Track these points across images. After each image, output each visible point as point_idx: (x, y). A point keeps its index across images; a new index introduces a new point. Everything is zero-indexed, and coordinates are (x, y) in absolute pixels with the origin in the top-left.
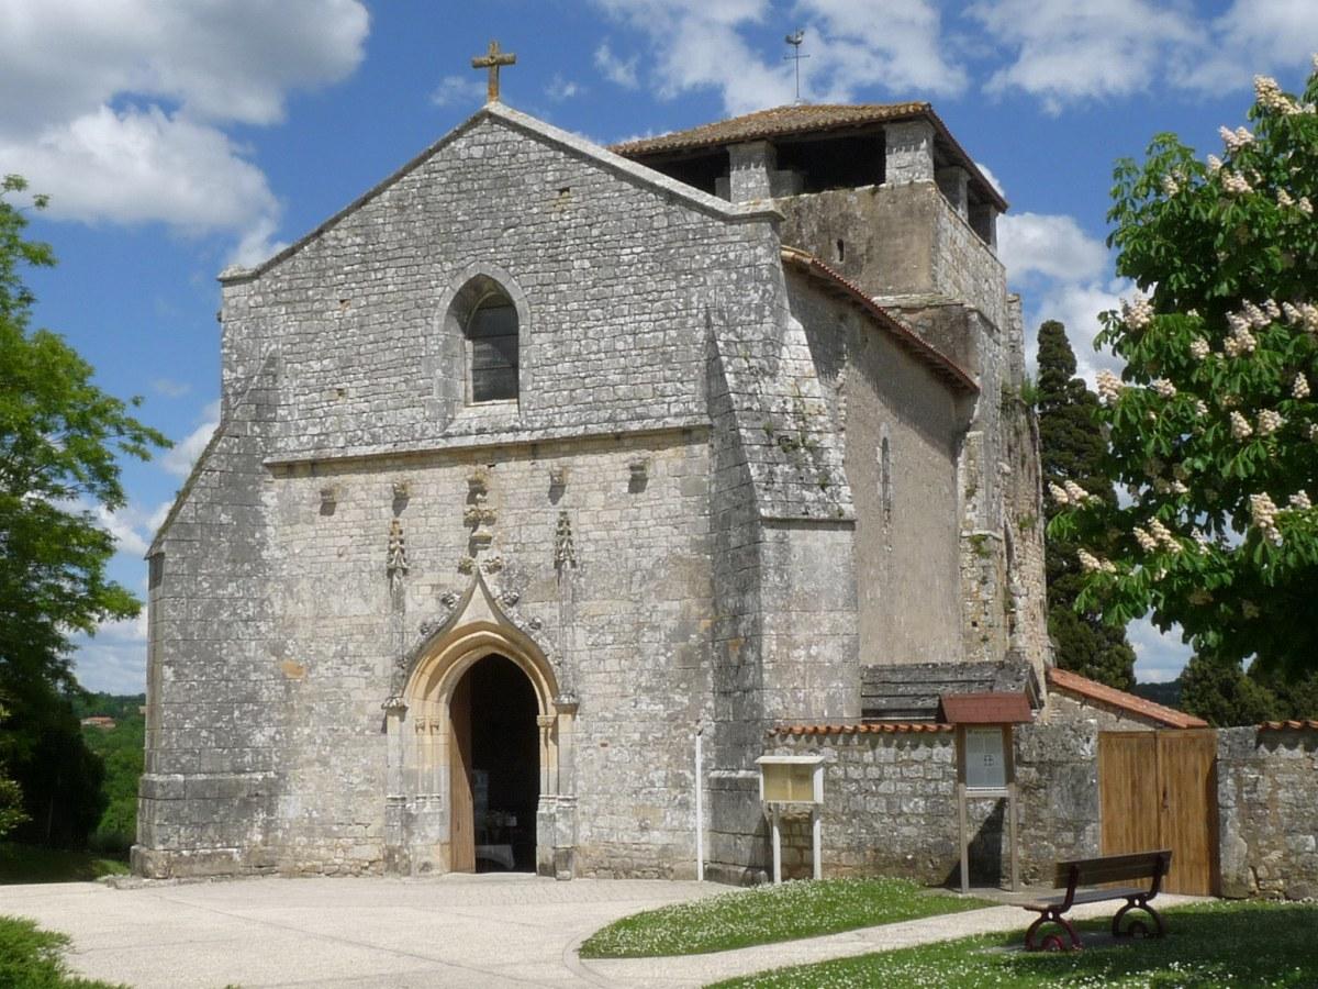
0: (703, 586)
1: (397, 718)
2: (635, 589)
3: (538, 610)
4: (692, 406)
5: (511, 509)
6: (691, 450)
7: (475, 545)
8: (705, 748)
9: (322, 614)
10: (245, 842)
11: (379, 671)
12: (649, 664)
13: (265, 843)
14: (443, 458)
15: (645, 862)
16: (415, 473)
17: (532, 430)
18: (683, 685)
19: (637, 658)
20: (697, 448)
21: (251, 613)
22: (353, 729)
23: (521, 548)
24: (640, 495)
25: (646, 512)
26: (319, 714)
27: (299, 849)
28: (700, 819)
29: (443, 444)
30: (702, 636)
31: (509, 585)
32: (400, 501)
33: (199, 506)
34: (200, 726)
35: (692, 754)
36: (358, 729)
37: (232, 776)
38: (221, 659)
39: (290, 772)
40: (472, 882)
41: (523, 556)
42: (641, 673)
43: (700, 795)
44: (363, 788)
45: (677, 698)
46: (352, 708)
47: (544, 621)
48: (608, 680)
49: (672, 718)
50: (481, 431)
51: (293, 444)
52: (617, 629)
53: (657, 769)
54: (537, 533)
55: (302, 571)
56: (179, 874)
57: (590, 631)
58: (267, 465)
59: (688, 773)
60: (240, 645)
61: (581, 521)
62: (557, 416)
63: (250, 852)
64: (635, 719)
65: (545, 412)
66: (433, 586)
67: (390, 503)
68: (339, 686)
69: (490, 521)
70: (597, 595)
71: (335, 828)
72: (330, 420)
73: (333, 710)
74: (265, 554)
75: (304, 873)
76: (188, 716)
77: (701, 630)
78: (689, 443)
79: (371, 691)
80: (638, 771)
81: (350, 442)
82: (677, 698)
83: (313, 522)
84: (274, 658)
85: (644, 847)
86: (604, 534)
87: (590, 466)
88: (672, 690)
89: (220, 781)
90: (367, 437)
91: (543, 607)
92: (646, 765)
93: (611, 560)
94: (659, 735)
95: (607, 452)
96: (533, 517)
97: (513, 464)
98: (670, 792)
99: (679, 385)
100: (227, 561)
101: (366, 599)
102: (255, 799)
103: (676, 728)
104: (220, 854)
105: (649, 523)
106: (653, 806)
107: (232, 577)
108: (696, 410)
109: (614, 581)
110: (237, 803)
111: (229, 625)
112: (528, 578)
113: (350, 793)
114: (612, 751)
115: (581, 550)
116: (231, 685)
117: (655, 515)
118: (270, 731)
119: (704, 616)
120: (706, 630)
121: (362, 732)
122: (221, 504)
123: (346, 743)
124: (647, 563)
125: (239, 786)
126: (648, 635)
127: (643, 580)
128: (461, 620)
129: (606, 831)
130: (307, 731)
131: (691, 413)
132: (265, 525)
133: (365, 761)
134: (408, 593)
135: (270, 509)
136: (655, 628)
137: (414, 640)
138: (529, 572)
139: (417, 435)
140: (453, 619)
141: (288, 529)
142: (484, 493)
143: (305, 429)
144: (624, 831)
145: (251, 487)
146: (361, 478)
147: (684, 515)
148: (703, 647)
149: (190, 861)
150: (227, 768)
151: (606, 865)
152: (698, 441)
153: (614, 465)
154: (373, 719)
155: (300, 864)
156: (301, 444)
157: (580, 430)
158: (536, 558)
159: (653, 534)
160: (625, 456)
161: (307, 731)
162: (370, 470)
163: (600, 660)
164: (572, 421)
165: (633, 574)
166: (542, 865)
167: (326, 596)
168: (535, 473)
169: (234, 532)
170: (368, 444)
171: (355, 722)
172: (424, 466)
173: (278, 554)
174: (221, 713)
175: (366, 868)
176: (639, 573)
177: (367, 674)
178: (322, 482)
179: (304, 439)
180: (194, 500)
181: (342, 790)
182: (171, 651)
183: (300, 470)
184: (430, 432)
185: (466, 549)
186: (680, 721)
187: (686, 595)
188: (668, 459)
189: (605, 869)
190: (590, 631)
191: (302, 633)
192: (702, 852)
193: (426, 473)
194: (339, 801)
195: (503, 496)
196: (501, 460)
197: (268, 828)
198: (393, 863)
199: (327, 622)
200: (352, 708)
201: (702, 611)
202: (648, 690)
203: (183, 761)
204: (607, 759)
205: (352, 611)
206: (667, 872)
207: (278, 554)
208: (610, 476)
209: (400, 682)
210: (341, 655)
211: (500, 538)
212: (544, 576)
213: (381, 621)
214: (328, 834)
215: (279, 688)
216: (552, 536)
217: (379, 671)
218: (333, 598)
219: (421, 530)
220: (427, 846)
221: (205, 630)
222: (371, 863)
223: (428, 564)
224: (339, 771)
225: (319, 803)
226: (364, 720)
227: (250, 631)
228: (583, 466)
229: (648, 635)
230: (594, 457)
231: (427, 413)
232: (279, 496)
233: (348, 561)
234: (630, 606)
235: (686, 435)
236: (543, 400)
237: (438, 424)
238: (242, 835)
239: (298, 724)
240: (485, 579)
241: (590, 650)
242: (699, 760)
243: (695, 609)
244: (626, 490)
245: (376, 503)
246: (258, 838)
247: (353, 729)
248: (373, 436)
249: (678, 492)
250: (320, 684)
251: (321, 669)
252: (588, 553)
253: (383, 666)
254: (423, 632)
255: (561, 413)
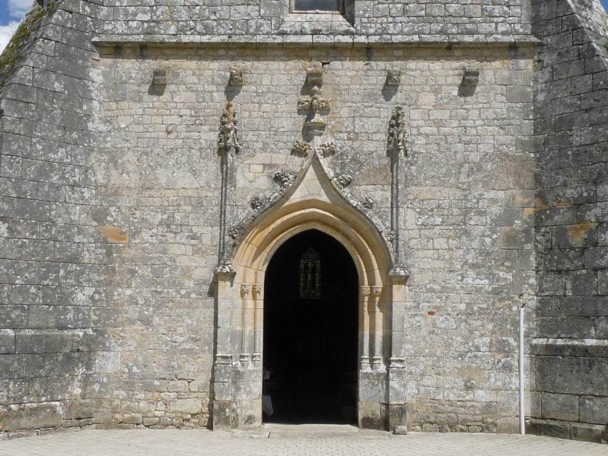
0: (529, 180)
1: (228, 283)
2: (463, 178)
3: (371, 192)
4: (518, 27)
5: (344, 102)
6: (517, 65)
7: (308, 132)
8: (528, 318)
9: (148, 184)
10: (67, 396)
11: (207, 240)
12: (476, 244)
13: (83, 396)
14: (278, 53)
15: (469, 417)
16: (248, 64)
17: (368, 35)
18: (507, 264)
19: (464, 238)
20: (522, 62)
21: (77, 179)
22: (178, 292)
23: (354, 136)
24: (469, 99)
25: (474, 114)
26: (142, 277)
27: (117, 402)
28: (523, 380)
29: (279, 39)
30: (524, 222)
31: (342, 168)
32: (233, 86)
33: (36, 71)
34: (30, 283)
35: (516, 324)
36: (183, 292)
37: (57, 333)
38: (50, 220)
39: (110, 330)
40: (334, 435)
41: (356, 144)
42: (467, 251)
43: (524, 360)
44: (188, 346)
45: (501, 274)
46: (178, 272)
47: (376, 202)
48: (436, 256)
49: (496, 292)
50: (315, 32)
51: (121, 27)
52: (446, 212)
53: (482, 335)
54: (370, 125)
55: (128, 145)
56: (7, 428)
57: (419, 213)
58: (95, 44)
59: (511, 340)
60: (66, 209)
61: (413, 117)
62: (391, 25)
63: (71, 406)
64: (461, 291)
65: (380, 20)
66: (265, 165)
67: (223, 88)
68: (164, 252)
69: (325, 111)
70: (427, 182)
71: (157, 383)
72: (161, 9)
73: (157, 273)
74: (90, 126)
75: (121, 425)
76: (19, 272)
77: (525, 217)
78: (515, 57)
79: (197, 258)
80: (463, 337)
81: (182, 31)
82: (501, 274)
83: (140, 100)
84: (94, 223)
85: (468, 404)
86: (435, 130)
87: (422, 71)
88: (497, 267)
89: (47, 336)
90: (199, 27)
91: (375, 190)
92: (471, 332)
93: (441, 152)
94: (484, 306)
95: (438, 60)
96: (367, 110)
97: (347, 63)
98: (493, 356)
99: (506, 8)
100: (59, 128)
101: (194, 173)
102: (76, 355)
103: (501, 300)
104: (44, 408)
105: (478, 122)
106: (478, 368)
107: (63, 143)
108: (521, 30)
109: (444, 171)
110: (60, 358)
111: (58, 188)
112: (361, 164)
113: (174, 349)
114: (439, 319)
115: (412, 143)
116: (58, 245)
117: (483, 116)
118: (89, 291)
119: (528, 205)
120: (530, 216)
121: (188, 295)
122: (55, 72)
123: (170, 305)
124: (475, 157)
125: (63, 341)
126: (475, 220)
127: (471, 172)
128: (292, 197)
129: (432, 389)
130: (128, 292)
131: (517, 33)
132: (92, 99)
133: (190, 322)
134: (239, 169)
135: (96, 85)
136: (481, 213)
137: (242, 214)
138: (362, 158)
139: (251, 30)
140: (286, 196)
141: (114, 105)
142: (320, 86)
143: (135, 15)
144: (449, 390)
145: (80, 62)
146: (193, 64)
147: (509, 118)
148: (526, 231)
149: (18, 415)
150: (52, 324)
151: (432, 419)
152: (523, 56)
153: (447, 71)
154: (199, 283)
155: (117, 416)
156: (129, 28)
157: (416, 38)
158: (369, 147)
159: (480, 132)
160: (455, 64)
161: (128, 292)
162: (201, 58)
163: (429, 239)
164: (406, 30)
165: (461, 165)
166: (364, 419)
167: (153, 169)
168: (370, 73)
169: (66, 101)
170: (199, 34)
171: (181, 285)
172: (258, 58)
173: (102, 127)
174: (48, 272)
175: (188, 420)
176: (467, 165)
177: (193, 242)
178: (152, 64)
179: (134, 24)
180: (32, 64)
181: (165, 348)
182: (6, 207)
183: (128, 51)
184: (266, 28)
185: (300, 134)
186: (504, 295)
187: (511, 186)
188: (496, 70)
189: (431, 423)
190: (419, 213)
191: (126, 201)
192: (525, 408)
193: (261, 65)
194: (162, 358)
195: (337, 89)
196: (335, 59)
197: (86, 382)
198: (215, 416)
199: (153, 193)
200: (178, 272)
201: (526, 201)
202: (474, 266)
203: (13, 316)
204: (434, 325)
205: (180, 184)
206: (491, 426)
207: (102, 127)
208: (441, 80)
209: (224, 253)
210: (167, 224)
211: (333, 126)
212: (377, 163)
213: (210, 194)
214: (149, 388)
215: (99, 251)
216: (385, 128)
217: (207, 240)
218: (160, 171)
219: (255, 114)
220: (251, 401)
221: (37, 190)
222: (193, 415)
223: (259, 145)
224: (162, 330)
225: (140, 359)
226: (190, 284)
227: (76, 196)
228: (416, 69)
229: (475, 220)
230: (426, 63)
231: (262, 12)
232: (104, 74)
233: (177, 137)
234: (459, 193)
235: (513, 50)
236: (378, 9)
237: (274, 22)
238: (64, 389)
239: (119, 285)
240: (321, 161)
241: (420, 230)
242: (523, 329)
243: (519, 199)
244: (455, 92)
245: (208, 88)
246: (78, 391)
247: (178, 292)
248: (206, 27)
249: (504, 98)
250: (143, 249)
251: (146, 235)
252: (419, 144)
253: (210, 235)
254: (253, 206)
255: (395, 23)
